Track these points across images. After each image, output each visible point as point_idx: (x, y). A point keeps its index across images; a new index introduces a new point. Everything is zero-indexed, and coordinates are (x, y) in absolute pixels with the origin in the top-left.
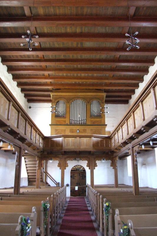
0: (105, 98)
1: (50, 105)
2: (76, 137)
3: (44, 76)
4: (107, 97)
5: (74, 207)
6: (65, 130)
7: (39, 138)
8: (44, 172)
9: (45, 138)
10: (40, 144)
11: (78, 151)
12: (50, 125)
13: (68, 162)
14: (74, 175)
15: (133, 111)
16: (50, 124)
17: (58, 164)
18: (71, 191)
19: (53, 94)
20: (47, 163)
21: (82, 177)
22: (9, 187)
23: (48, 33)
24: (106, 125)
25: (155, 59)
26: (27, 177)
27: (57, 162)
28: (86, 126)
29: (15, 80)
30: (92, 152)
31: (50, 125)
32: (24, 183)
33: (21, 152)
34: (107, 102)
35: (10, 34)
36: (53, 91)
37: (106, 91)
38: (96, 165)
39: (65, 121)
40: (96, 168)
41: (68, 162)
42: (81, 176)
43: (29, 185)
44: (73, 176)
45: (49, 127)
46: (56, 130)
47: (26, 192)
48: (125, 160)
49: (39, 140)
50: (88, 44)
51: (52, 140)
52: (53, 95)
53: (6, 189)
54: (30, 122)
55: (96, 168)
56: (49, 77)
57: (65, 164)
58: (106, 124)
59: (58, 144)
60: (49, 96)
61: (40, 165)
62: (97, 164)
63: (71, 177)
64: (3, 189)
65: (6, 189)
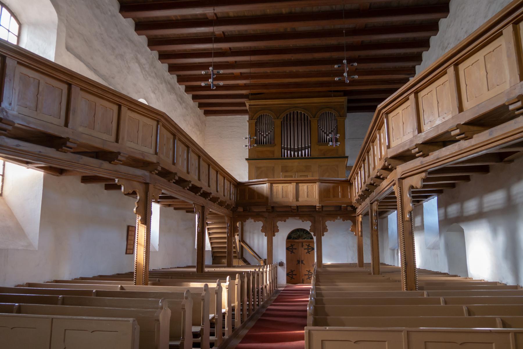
0: (346, 104)
1: (247, 117)
2: (291, 183)
3: (234, 74)
4: (349, 101)
5: (99, 95)
6: (274, 167)
7: (229, 185)
8: (291, 279)
9: (239, 185)
10: (232, 196)
11: (293, 207)
12: (246, 159)
13: (279, 224)
14: (292, 246)
15: (366, 150)
16: (248, 158)
17: (262, 227)
18: (288, 275)
19: (252, 103)
20: (519, 26)
21: (308, 249)
22: (183, 266)
23: (234, 17)
24: (347, 157)
25: (430, 39)
26: (211, 249)
27: (260, 224)
28: (311, 160)
29: (182, 83)
30: (317, 207)
31: (246, 159)
32: (208, 260)
33: (205, 212)
34: (351, 109)
35: (173, 20)
36: (250, 97)
37: (346, 93)
38: (325, 229)
39: (273, 152)
40: (325, 233)
41: (279, 224)
42: (306, 247)
43: (214, 263)
44: (291, 248)
45: (246, 164)
46: (258, 168)
47: (213, 271)
48: (385, 219)
49: (229, 189)
50: (301, 26)
51: (250, 189)
52: (250, 105)
53: (178, 268)
54: (214, 165)
55: (325, 233)
56: (242, 76)
57: (274, 227)
58: (346, 155)
59: (259, 195)
60: (244, 104)
61: (233, 231)
62: (327, 228)
63: (287, 249)
64: (175, 268)
65: (178, 268)
